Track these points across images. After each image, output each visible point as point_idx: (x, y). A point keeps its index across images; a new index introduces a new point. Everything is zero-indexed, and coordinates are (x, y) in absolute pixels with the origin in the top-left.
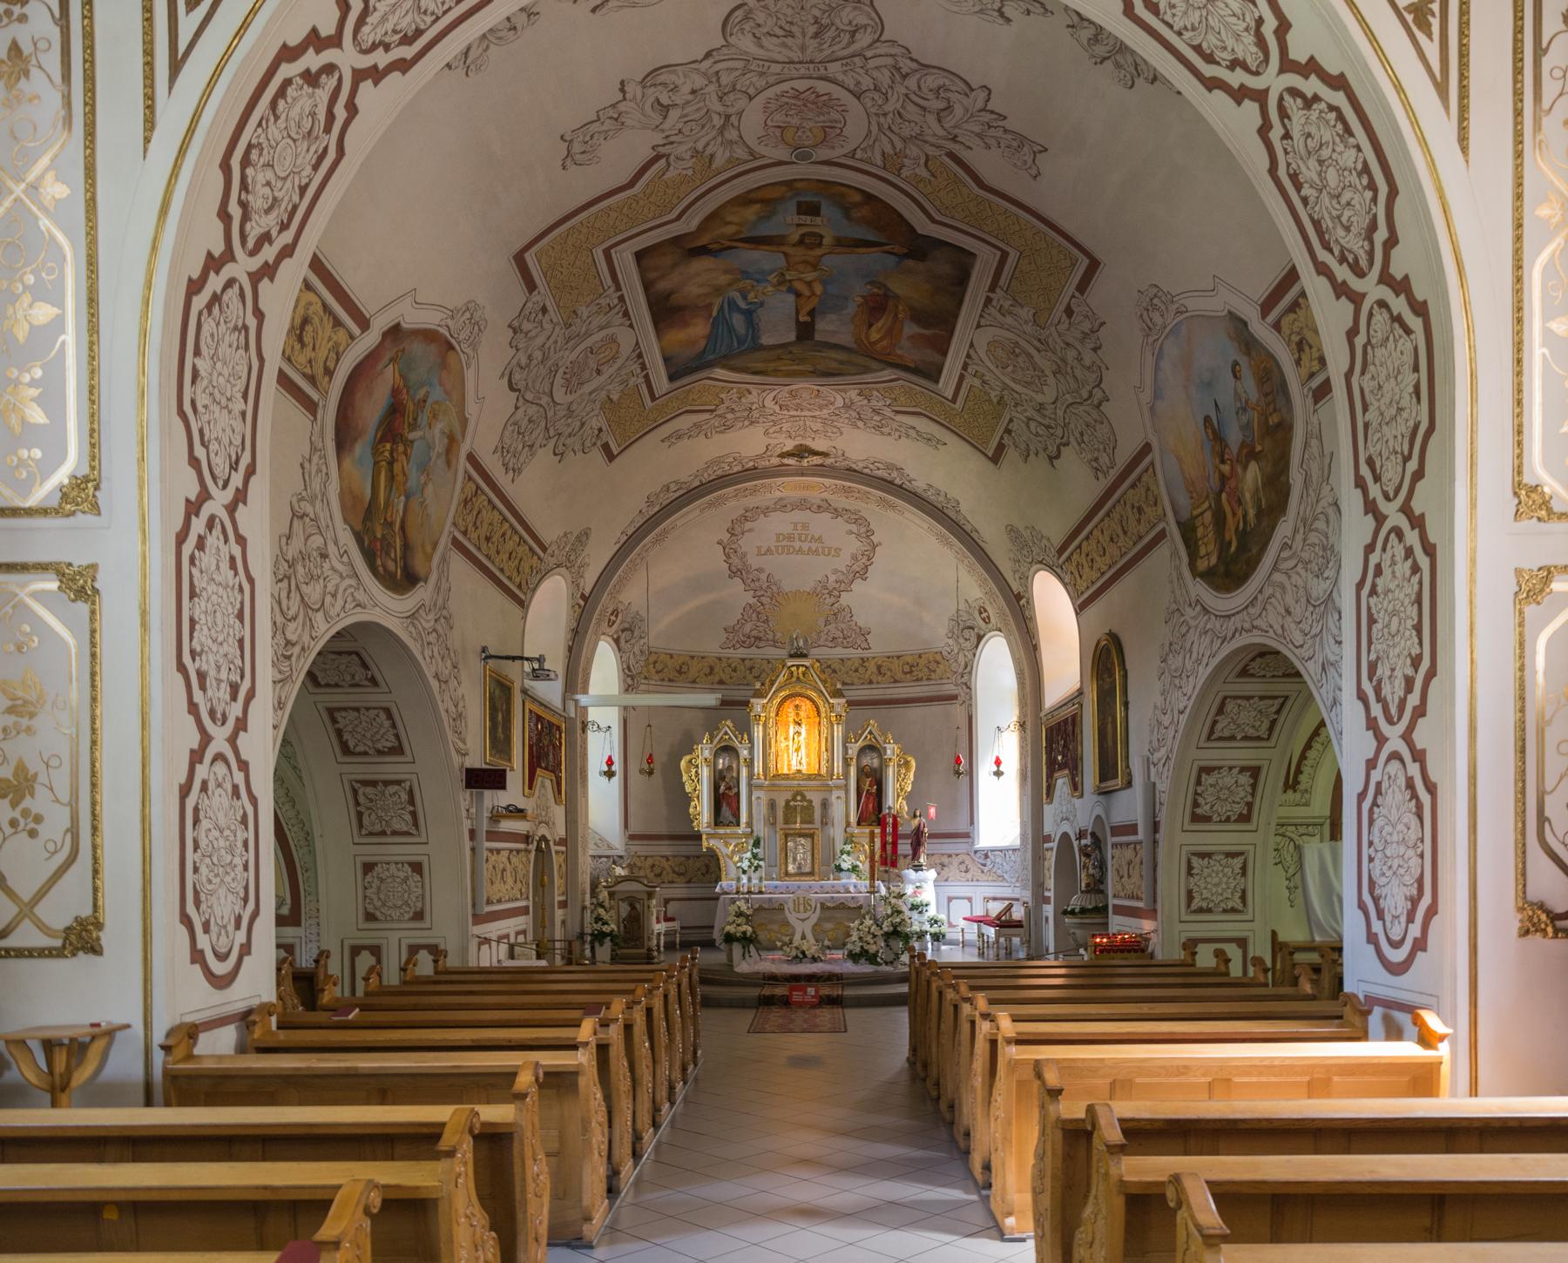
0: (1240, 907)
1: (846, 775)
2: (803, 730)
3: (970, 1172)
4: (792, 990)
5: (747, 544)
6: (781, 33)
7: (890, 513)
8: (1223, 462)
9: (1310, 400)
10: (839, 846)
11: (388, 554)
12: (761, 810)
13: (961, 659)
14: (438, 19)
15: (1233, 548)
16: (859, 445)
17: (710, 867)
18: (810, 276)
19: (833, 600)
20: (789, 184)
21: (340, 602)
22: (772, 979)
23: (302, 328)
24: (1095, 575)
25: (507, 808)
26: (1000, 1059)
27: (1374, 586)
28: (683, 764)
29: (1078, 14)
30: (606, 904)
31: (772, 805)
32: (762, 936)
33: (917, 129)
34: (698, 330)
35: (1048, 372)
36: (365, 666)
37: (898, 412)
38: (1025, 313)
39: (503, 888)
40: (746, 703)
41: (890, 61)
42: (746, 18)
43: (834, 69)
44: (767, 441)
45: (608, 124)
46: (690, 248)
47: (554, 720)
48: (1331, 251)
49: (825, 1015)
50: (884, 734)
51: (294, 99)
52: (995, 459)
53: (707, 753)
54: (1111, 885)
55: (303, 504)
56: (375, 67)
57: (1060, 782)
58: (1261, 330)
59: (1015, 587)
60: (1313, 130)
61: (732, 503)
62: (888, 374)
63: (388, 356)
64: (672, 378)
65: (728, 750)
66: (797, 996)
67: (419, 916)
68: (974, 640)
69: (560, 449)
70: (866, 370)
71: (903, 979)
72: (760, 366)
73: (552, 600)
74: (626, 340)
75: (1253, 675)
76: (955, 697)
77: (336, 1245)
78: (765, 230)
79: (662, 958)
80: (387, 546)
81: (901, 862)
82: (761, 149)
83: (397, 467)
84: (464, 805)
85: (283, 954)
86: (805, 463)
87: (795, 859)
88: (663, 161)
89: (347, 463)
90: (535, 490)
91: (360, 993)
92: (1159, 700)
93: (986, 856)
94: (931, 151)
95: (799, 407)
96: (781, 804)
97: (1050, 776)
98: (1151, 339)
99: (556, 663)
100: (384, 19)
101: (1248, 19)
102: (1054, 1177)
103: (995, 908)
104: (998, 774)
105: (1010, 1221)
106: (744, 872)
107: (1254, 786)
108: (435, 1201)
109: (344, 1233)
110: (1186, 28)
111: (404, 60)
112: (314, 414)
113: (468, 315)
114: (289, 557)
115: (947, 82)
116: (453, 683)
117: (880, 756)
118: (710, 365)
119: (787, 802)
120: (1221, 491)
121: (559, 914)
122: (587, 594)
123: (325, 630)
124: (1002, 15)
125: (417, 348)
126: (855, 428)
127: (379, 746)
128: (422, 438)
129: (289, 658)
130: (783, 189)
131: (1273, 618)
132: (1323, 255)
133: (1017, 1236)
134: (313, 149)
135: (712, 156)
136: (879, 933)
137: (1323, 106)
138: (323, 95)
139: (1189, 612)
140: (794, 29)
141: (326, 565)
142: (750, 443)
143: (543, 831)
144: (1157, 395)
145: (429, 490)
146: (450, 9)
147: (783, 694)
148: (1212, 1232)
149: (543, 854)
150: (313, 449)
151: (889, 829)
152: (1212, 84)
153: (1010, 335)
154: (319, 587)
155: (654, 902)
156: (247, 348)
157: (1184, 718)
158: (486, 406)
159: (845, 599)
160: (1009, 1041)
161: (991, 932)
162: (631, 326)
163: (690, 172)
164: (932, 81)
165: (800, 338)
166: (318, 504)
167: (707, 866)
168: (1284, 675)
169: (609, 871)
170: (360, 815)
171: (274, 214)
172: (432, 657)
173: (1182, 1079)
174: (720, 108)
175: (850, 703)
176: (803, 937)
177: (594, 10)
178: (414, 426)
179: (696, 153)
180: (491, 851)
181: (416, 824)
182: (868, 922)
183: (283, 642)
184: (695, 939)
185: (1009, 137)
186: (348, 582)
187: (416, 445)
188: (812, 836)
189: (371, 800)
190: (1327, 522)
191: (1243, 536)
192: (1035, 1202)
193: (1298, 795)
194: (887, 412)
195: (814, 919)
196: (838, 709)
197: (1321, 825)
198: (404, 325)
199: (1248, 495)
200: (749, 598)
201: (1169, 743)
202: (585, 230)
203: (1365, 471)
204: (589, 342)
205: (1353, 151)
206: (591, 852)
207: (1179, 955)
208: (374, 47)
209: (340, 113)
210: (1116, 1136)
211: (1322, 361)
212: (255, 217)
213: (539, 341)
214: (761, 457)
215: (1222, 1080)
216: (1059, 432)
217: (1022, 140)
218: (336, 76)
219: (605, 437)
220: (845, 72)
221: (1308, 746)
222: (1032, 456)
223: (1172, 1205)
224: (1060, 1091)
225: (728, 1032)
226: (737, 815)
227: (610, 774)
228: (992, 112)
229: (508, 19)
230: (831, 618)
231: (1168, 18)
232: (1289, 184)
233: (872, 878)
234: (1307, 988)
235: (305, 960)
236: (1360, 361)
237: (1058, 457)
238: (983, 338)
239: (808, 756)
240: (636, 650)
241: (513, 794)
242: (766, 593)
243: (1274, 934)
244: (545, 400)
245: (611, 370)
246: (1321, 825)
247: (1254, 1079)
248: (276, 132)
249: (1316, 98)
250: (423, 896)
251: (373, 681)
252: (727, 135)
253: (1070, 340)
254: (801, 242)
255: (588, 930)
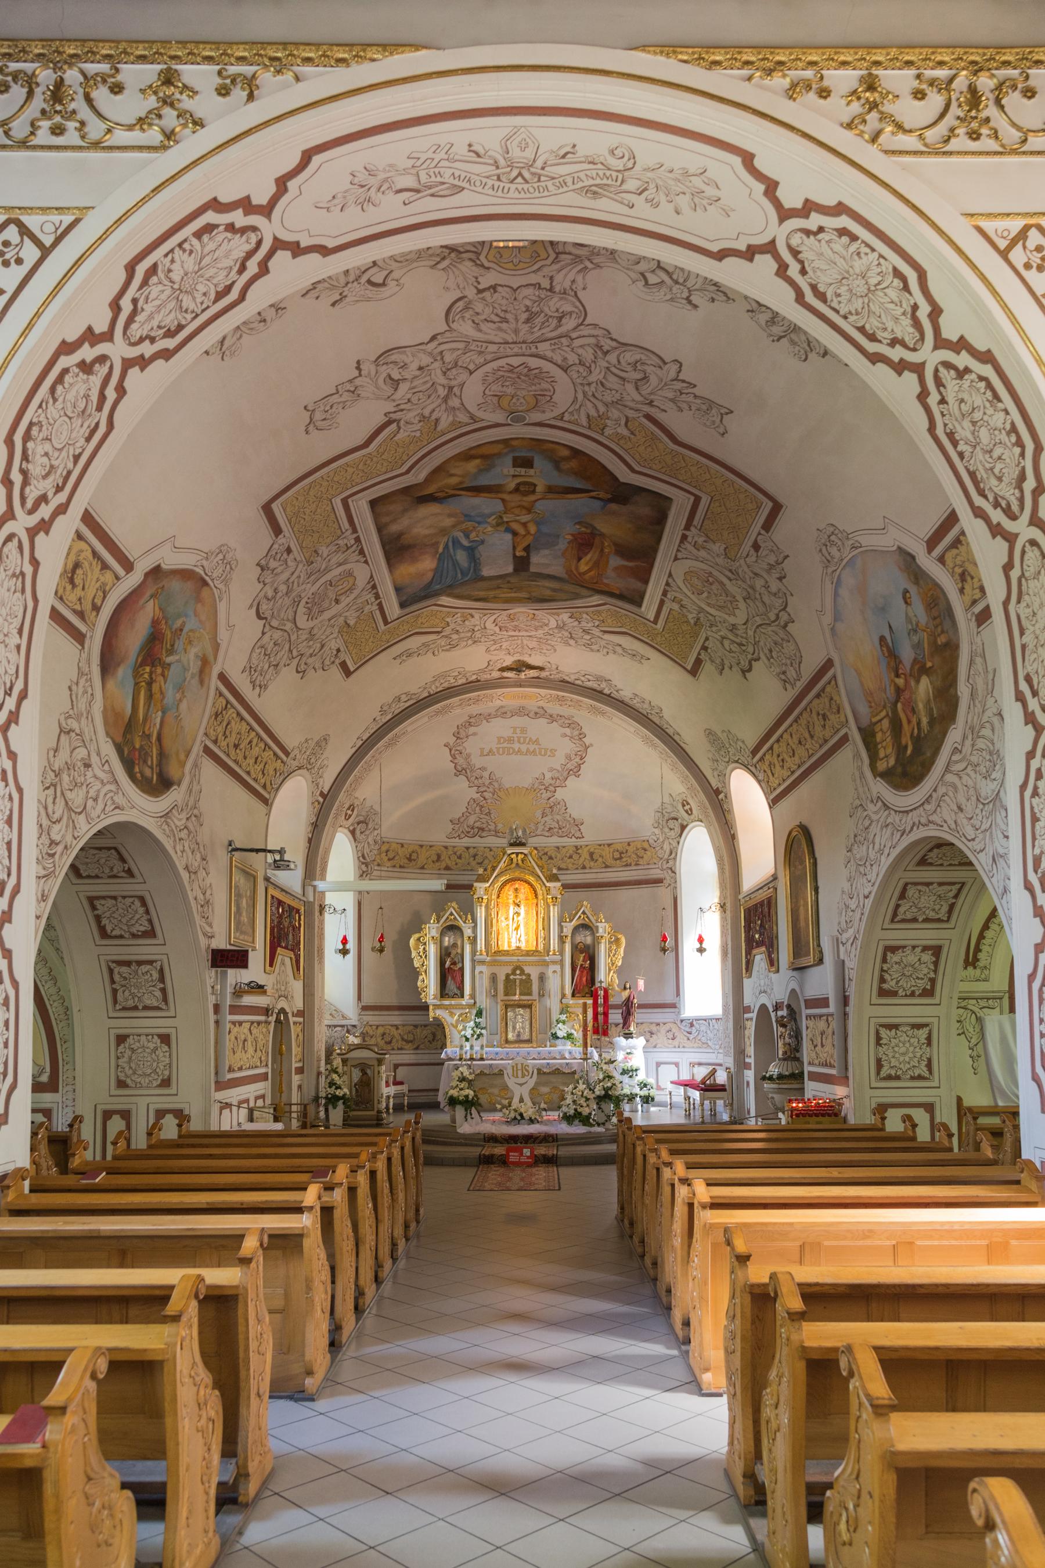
0: (927, 1074)
1: (562, 952)
2: (522, 910)
3: (671, 1327)
4: (509, 1150)
5: (471, 746)
6: (497, 319)
7: (600, 719)
8: (898, 676)
9: (973, 624)
10: (555, 1015)
11: (145, 762)
12: (484, 983)
13: (666, 847)
14: (197, 316)
15: (909, 752)
16: (572, 660)
17: (437, 1035)
18: (525, 518)
19: (549, 794)
20: (506, 442)
21: (100, 806)
22: (492, 1139)
23: (73, 571)
24: (786, 773)
25: (248, 984)
26: (696, 1222)
27: (1036, 788)
28: (412, 942)
29: (758, 302)
30: (340, 1070)
31: (494, 978)
32: (483, 1099)
33: (618, 396)
34: (427, 565)
35: (739, 598)
36: (123, 860)
37: (605, 632)
38: (718, 548)
39: (244, 1057)
40: (470, 887)
41: (592, 340)
42: (467, 308)
43: (544, 348)
44: (488, 657)
45: (346, 396)
46: (419, 496)
47: (294, 904)
48: (985, 497)
49: (541, 1173)
50: (596, 914)
51: (71, 385)
52: (694, 672)
53: (434, 933)
54: (807, 1052)
55: (70, 721)
56: (142, 356)
57: (758, 958)
58: (927, 563)
59: (715, 783)
60: (966, 396)
61: (458, 711)
62: (596, 599)
63: (148, 594)
64: (402, 605)
65: (452, 928)
66: (513, 1157)
67: (166, 1083)
68: (678, 830)
69: (303, 667)
70: (577, 596)
71: (613, 1139)
72: (482, 594)
73: (294, 799)
74: (361, 575)
75: (931, 864)
76: (659, 881)
77: (62, 1410)
78: (485, 480)
79: (391, 1119)
80: (144, 755)
81: (612, 1030)
82: (480, 414)
83: (155, 687)
84: (210, 982)
85: (40, 1118)
86: (522, 676)
87: (514, 1028)
88: (394, 426)
89: (111, 684)
90: (281, 704)
91: (109, 1158)
92: (846, 886)
93: (692, 1025)
94: (631, 414)
95: (516, 629)
96: (501, 978)
97: (748, 952)
98: (830, 570)
99: (296, 855)
100: (151, 317)
101: (904, 305)
102: (743, 1338)
103: (701, 1073)
104: (701, 950)
105: (707, 1378)
106: (467, 1040)
107: (936, 964)
108: (161, 1363)
109: (70, 1400)
110: (850, 313)
111: (167, 350)
112: (82, 644)
113: (221, 556)
114: (56, 768)
115: (643, 357)
116: (202, 874)
117: (593, 934)
118: (437, 594)
119: (508, 976)
120: (897, 702)
121: (296, 1079)
122: (326, 791)
123: (86, 830)
124: (690, 302)
125: (175, 585)
126: (565, 643)
127: (134, 930)
128: (179, 661)
129: (53, 855)
130: (501, 446)
131: (947, 813)
132: (979, 501)
133: (713, 1391)
134: (86, 425)
135: (437, 420)
136: (591, 1096)
137: (973, 376)
138: (96, 381)
139: (871, 808)
140: (509, 316)
141: (89, 774)
142: (473, 659)
143: (282, 1004)
144: (837, 617)
145: (184, 706)
146: (208, 307)
147: (503, 879)
148: (881, 1402)
149: (281, 1024)
150: (81, 673)
151: (601, 1001)
152: (875, 358)
153: (705, 567)
154: (81, 793)
155: (383, 1068)
156: (23, 591)
157: (869, 903)
158: (237, 633)
159: (560, 794)
160: (704, 1207)
161: (696, 1095)
162: (366, 562)
163: (418, 434)
164: (629, 357)
165: (516, 570)
166: (83, 720)
167: (434, 1035)
168: (960, 864)
169: (343, 1039)
170: (115, 992)
171: (51, 479)
172: (183, 852)
173: (868, 1242)
174: (445, 382)
175: (565, 886)
176: (521, 1100)
177: (333, 305)
178: (171, 652)
179: (423, 418)
180: (234, 1023)
181: (165, 1000)
182: (582, 1086)
183: (48, 842)
184: (422, 1102)
185: (698, 401)
186: (108, 787)
187: (173, 667)
188: (530, 1006)
189: (125, 978)
190: (993, 730)
191: (917, 740)
192: (727, 1361)
193: (978, 971)
194: (596, 632)
195: (531, 1083)
196: (554, 892)
197: (1001, 999)
198: (163, 566)
199: (921, 706)
200: (473, 793)
201: (856, 925)
202: (325, 484)
203: (1024, 686)
204: (328, 577)
205: (1002, 414)
206: (327, 1022)
207: (869, 1120)
208: (141, 340)
209: (111, 394)
210: (796, 1304)
211: (982, 589)
212: (33, 482)
213: (285, 576)
214: (483, 671)
215: (904, 1244)
216: (750, 649)
217: (711, 404)
218: (108, 364)
219: (343, 656)
220: (553, 350)
221: (986, 927)
222: (726, 668)
223: (845, 1374)
224: (748, 1257)
225: (446, 1186)
226: (461, 988)
227: (344, 952)
228: (683, 381)
229: (259, 313)
230: (548, 811)
231: (835, 305)
232: (947, 442)
233: (585, 1045)
234: (988, 1153)
235: (60, 1124)
236: (1015, 592)
237: (750, 670)
238: (679, 570)
239: (527, 934)
240: (371, 840)
241: (255, 971)
242: (489, 790)
243: (959, 1099)
244: (289, 626)
245: (348, 600)
246: (1001, 999)
247: (936, 1243)
248: (54, 412)
249: (967, 370)
250: (170, 1064)
251: (130, 873)
252: (451, 403)
253: (758, 571)
254: (517, 490)
255: (323, 1094)
